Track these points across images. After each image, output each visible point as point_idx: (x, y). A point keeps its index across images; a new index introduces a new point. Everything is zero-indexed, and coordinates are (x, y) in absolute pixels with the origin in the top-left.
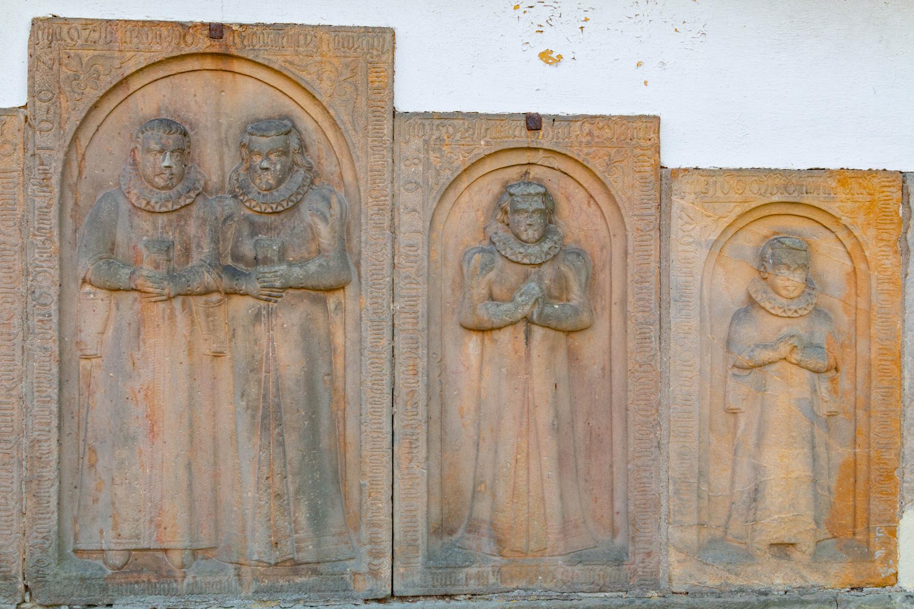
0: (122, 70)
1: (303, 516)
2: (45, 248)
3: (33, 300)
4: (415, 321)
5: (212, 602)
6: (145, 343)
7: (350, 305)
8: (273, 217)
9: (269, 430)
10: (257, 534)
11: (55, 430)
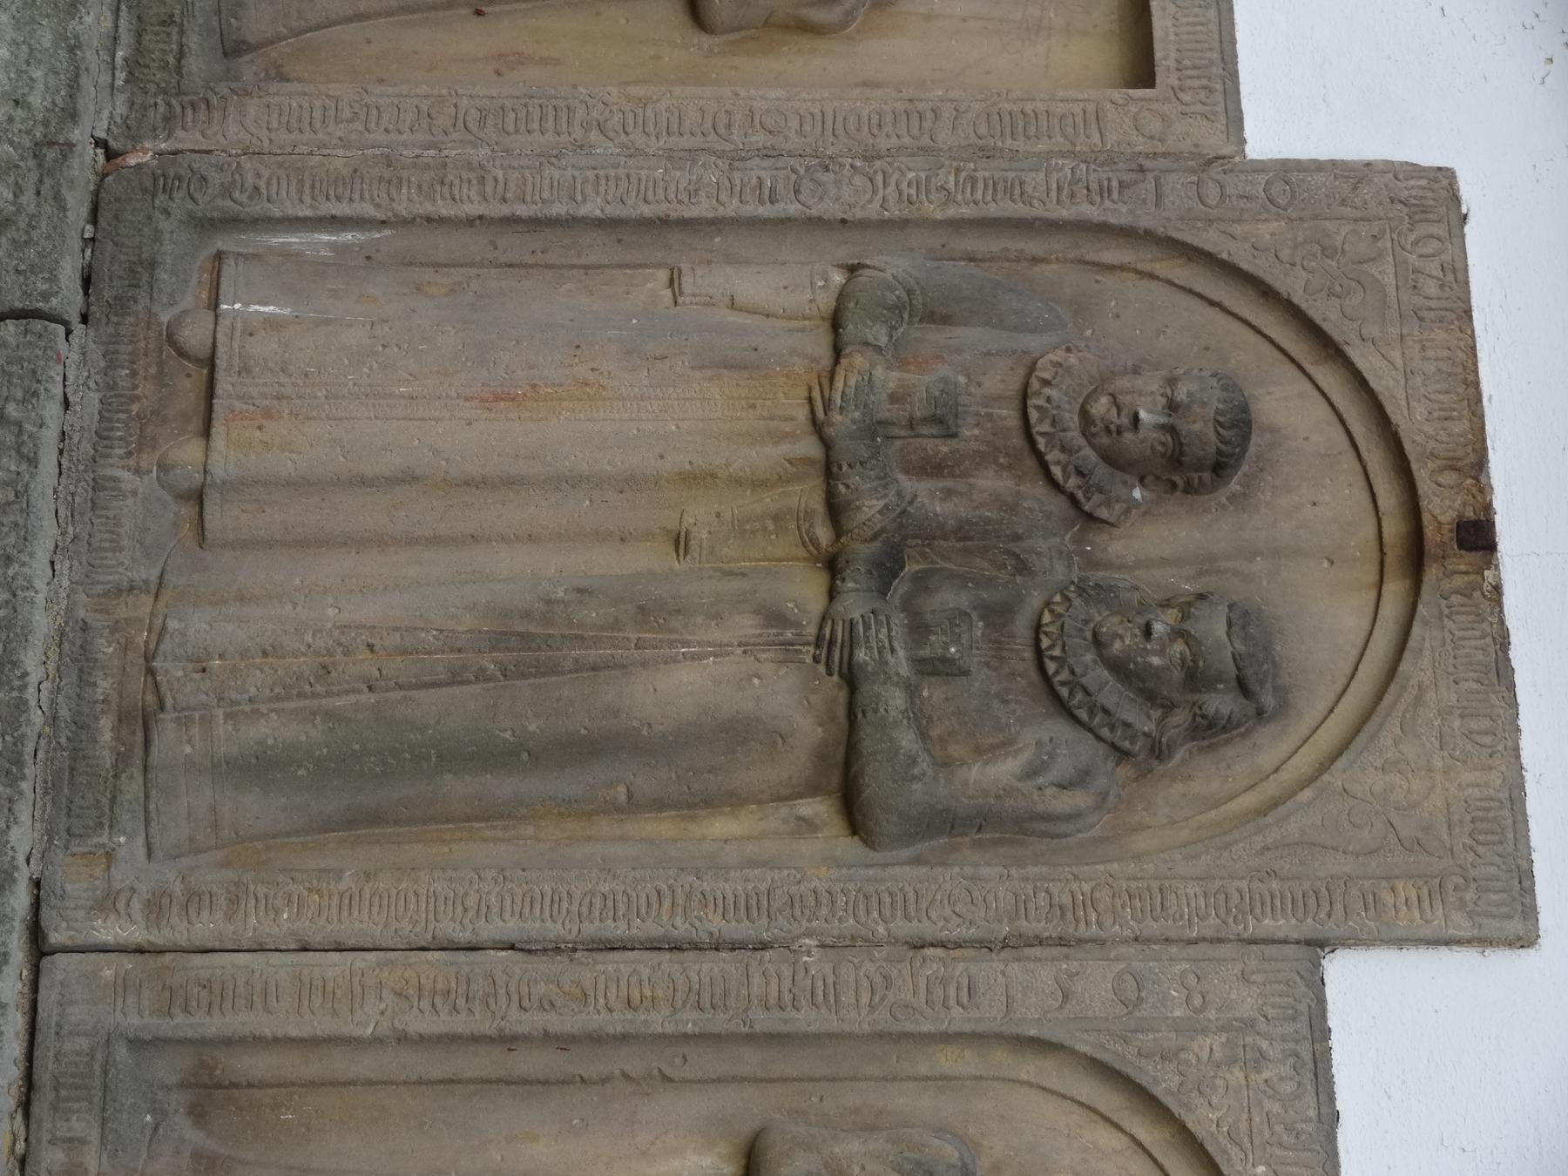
0: (1357, 341)
1: (270, 731)
2: (928, 192)
3: (808, 169)
4: (772, 1001)
5: (71, 530)
6: (711, 379)
7: (808, 847)
8: (1029, 654)
9: (493, 648)
10: (230, 627)
11: (505, 210)
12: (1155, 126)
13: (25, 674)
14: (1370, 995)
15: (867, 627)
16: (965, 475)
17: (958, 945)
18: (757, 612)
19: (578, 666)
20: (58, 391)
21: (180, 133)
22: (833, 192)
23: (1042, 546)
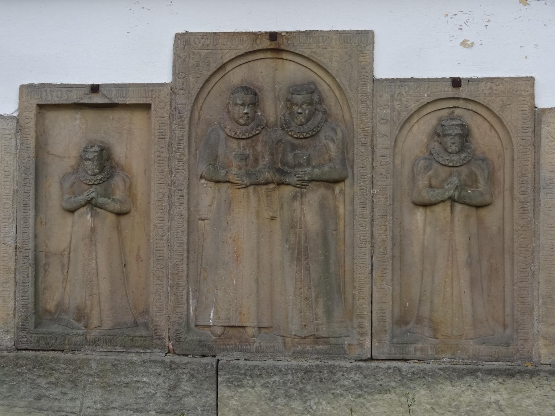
1: (320, 311)
8: (304, 140)
11: (185, 259)
12: (162, 104)
13: (309, 365)
14: (384, 69)
15: (299, 177)
16: (258, 153)
17: (373, 159)
18: (293, 202)
19: (306, 242)
20: (237, 362)
21: (163, 336)
22: (181, 182)
23: (274, 136)
